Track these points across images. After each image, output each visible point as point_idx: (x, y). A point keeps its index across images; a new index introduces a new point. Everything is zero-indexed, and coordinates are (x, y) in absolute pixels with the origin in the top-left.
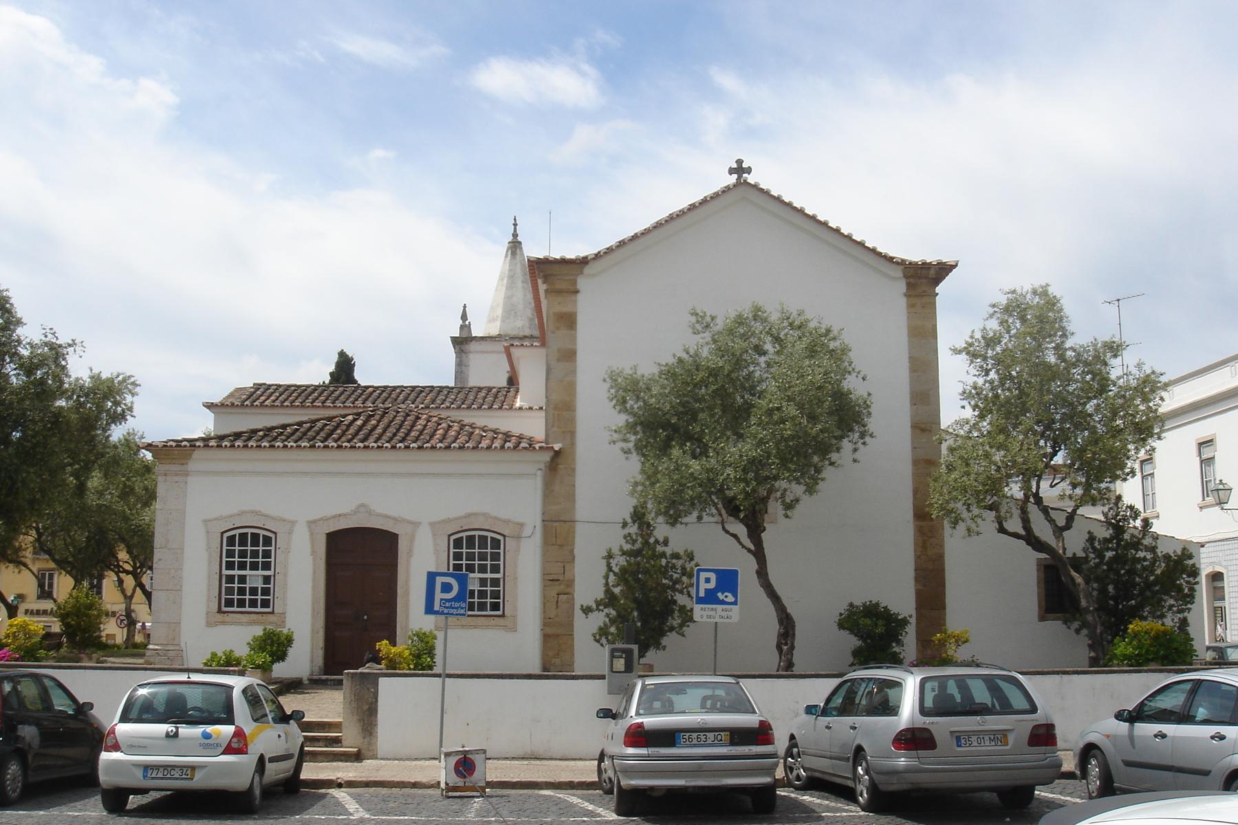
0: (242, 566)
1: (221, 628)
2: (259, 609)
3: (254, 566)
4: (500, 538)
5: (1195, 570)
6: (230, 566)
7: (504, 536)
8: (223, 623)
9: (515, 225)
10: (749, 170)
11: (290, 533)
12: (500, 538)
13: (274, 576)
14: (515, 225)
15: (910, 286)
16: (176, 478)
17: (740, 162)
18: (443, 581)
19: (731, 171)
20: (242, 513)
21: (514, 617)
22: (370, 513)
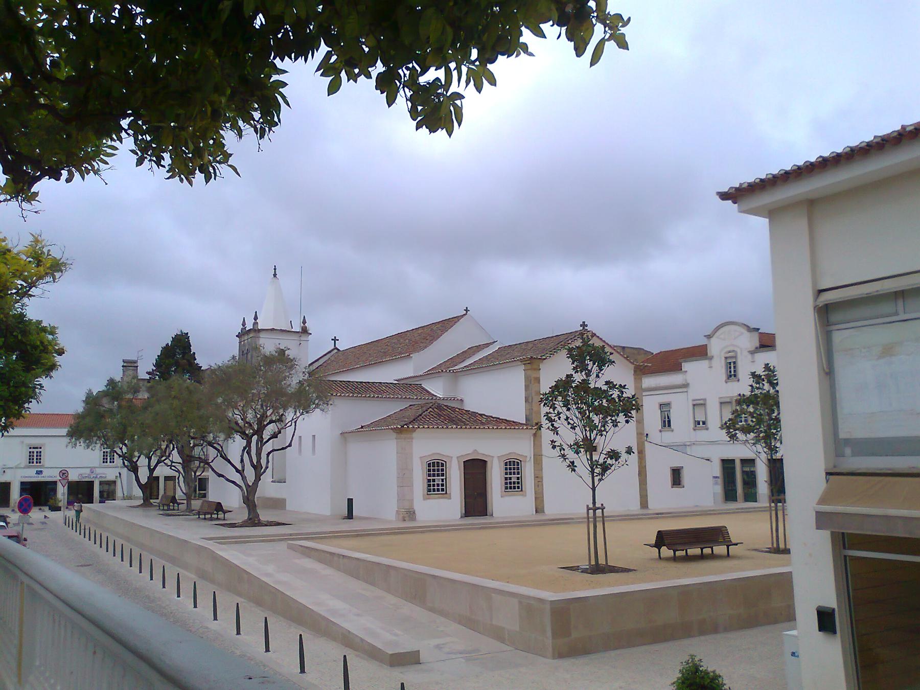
0: (434, 475)
1: (428, 501)
2: (436, 492)
3: (438, 475)
4: (519, 461)
5: (86, 441)
6: (429, 475)
7: (521, 461)
8: (429, 499)
9: (275, 269)
10: (587, 326)
11: (451, 461)
12: (519, 461)
13: (446, 479)
14: (275, 269)
15: (635, 371)
16: (409, 440)
17: (584, 322)
18: (101, 480)
19: (581, 326)
20: (434, 454)
21: (450, 494)
22: (478, 453)
